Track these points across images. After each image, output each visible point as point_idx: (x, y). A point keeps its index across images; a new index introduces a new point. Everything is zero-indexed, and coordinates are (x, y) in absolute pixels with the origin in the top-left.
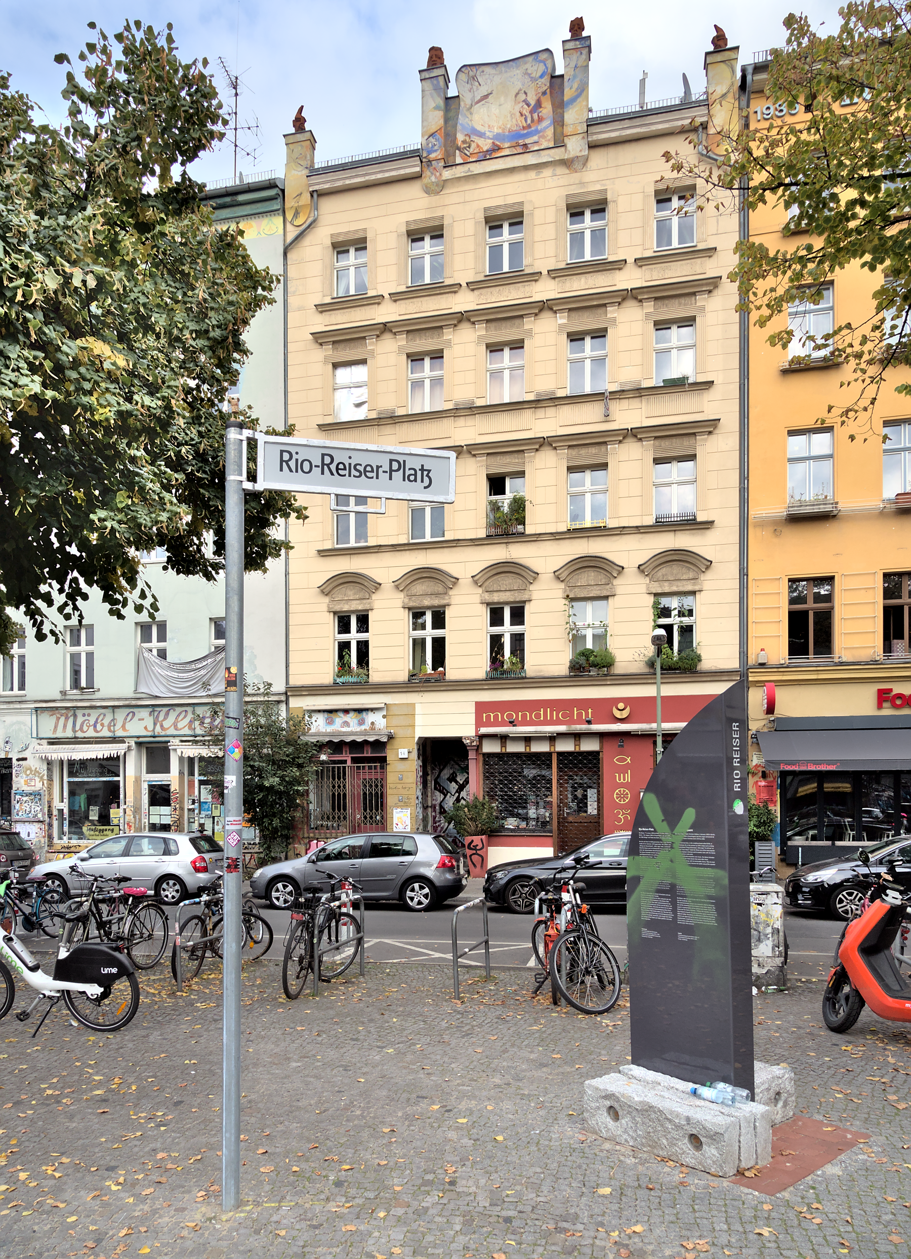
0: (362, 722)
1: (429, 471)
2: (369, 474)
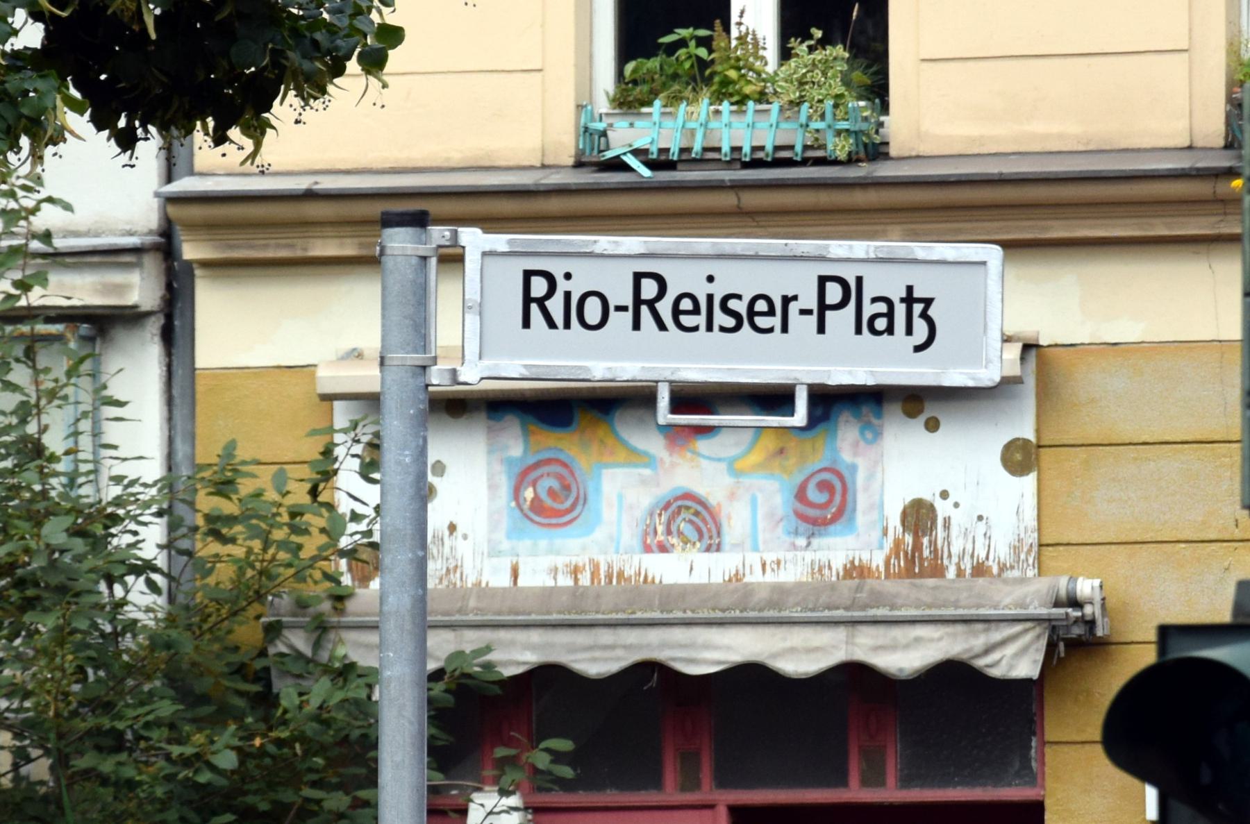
0: (823, 506)
1: (928, 302)
2: (761, 322)
